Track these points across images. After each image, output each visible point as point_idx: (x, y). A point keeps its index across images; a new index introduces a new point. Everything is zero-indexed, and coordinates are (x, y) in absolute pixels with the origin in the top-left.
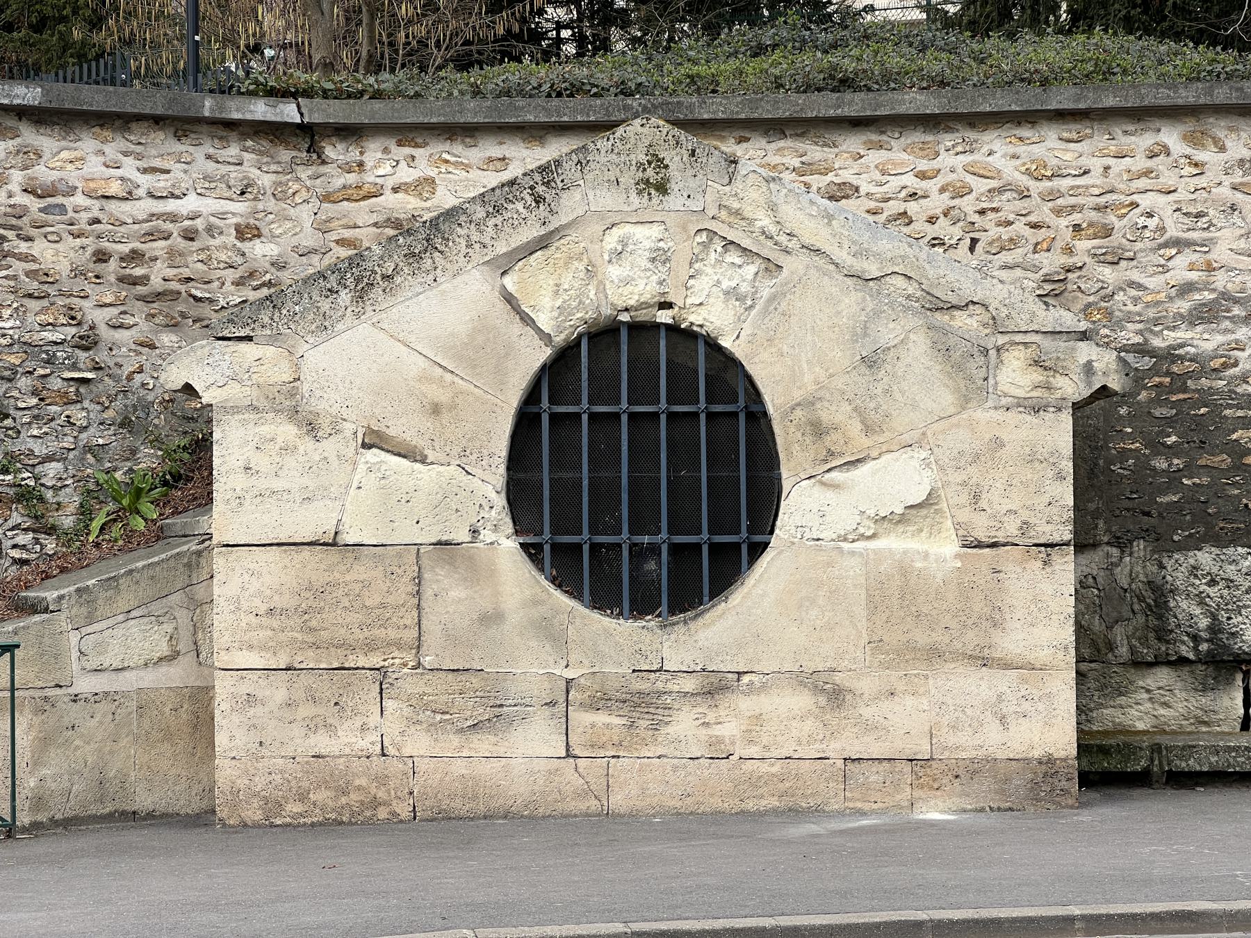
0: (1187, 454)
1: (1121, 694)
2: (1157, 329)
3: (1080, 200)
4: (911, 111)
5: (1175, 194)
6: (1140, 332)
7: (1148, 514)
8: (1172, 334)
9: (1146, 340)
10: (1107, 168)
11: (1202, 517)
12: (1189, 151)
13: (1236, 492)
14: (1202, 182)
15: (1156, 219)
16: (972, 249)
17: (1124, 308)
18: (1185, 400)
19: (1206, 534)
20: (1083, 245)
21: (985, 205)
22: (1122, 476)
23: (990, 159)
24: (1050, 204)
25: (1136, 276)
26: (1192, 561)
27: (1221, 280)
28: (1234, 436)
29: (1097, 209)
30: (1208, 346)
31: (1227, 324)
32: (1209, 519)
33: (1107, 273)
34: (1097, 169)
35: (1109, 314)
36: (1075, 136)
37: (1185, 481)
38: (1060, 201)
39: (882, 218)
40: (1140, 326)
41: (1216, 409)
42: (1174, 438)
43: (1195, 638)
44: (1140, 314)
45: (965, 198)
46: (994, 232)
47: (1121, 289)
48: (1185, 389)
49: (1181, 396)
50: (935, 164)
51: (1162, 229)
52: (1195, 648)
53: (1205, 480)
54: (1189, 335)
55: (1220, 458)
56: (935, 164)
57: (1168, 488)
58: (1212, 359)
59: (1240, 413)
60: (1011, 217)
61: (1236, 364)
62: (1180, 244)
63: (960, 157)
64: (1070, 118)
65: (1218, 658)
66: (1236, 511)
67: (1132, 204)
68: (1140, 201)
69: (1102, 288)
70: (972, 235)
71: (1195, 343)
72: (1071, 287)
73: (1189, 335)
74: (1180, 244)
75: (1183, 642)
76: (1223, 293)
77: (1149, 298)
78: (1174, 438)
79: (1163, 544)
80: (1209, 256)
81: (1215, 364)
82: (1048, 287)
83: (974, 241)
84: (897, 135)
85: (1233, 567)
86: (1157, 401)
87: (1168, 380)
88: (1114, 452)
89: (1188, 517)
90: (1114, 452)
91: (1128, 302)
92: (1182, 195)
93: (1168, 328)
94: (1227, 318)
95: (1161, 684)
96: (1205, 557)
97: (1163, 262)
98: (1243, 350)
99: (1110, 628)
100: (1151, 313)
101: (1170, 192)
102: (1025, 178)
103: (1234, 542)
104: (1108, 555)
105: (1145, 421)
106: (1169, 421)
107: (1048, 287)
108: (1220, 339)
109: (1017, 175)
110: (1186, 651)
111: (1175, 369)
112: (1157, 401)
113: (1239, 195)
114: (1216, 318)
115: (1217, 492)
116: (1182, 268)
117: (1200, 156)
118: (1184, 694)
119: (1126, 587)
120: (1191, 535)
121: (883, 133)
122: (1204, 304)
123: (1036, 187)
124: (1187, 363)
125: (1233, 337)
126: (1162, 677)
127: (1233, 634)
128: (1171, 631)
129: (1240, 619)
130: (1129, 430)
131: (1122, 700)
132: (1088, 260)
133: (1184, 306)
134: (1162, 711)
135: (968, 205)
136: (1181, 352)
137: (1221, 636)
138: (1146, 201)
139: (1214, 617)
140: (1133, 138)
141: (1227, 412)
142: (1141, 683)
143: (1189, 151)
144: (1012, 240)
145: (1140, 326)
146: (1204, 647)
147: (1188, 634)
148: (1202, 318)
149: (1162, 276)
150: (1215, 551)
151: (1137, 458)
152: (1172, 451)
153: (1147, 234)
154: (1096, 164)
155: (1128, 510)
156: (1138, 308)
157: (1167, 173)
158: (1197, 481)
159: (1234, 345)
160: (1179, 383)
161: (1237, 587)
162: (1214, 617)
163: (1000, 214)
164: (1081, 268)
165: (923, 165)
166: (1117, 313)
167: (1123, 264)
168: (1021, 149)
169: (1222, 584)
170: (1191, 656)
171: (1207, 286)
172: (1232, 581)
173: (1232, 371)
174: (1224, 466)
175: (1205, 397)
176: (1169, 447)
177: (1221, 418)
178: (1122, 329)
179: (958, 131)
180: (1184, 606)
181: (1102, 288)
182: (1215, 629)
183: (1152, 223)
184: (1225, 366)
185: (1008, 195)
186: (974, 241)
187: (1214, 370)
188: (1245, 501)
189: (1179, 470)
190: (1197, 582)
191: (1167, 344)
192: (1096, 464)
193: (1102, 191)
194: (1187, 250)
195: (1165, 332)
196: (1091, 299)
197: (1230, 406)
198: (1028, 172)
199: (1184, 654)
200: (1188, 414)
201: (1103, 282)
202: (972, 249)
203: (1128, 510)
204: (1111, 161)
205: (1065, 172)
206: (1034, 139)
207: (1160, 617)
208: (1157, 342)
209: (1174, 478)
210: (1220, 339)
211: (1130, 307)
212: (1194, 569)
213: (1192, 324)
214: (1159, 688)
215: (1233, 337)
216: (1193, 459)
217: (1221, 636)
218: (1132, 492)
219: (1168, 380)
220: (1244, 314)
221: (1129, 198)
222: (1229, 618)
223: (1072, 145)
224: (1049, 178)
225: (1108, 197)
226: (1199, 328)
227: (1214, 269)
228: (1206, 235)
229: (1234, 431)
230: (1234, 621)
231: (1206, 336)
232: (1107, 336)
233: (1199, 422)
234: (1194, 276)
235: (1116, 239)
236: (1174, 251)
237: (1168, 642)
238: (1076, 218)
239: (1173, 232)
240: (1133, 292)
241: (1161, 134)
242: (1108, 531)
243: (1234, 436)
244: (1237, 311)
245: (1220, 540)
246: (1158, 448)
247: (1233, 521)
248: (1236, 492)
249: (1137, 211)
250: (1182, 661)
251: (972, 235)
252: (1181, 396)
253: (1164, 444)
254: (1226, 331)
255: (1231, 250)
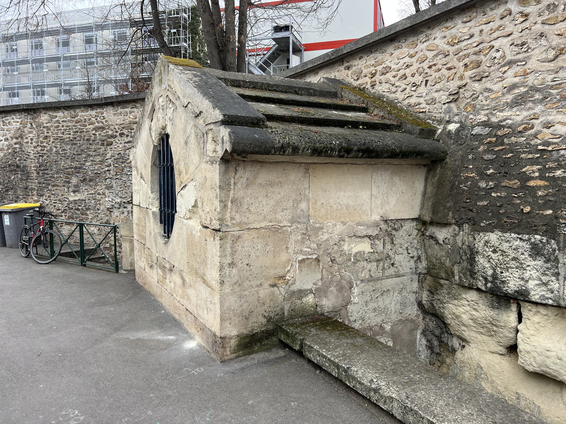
0: (497, 180)
1: (455, 299)
2: (495, 112)
3: (469, 51)
4: (401, 29)
5: (512, 36)
6: (487, 115)
7: (471, 211)
8: (501, 114)
9: (489, 119)
10: (481, 31)
11: (496, 215)
12: (521, 9)
13: (518, 202)
14: (526, 25)
15: (500, 53)
16: (426, 85)
17: (481, 103)
18: (502, 150)
19: (497, 224)
20: (469, 73)
21: (431, 64)
22: (464, 190)
23: (435, 41)
24: (456, 56)
25: (489, 85)
26: (486, 238)
27: (531, 80)
28: (524, 170)
29: (475, 54)
30: (519, 119)
31: (530, 104)
32: (500, 216)
33: (477, 86)
34: (477, 33)
35: (474, 107)
36: (468, 19)
37: (493, 194)
38: (461, 54)
39: (398, 78)
40: (487, 112)
41: (517, 154)
42: (491, 171)
43: (486, 279)
44: (488, 105)
45: (425, 62)
46: (434, 74)
47: (482, 93)
48: (502, 144)
49: (501, 148)
50: (416, 50)
51: (503, 57)
52: (486, 284)
53: (504, 194)
54: (510, 113)
55: (513, 182)
56: (416, 50)
57: (484, 198)
58: (520, 125)
59: (530, 156)
60: (440, 67)
61: (532, 128)
62: (511, 63)
63: (425, 44)
64: (467, 10)
65: (495, 293)
66: (516, 212)
67: (490, 47)
68: (494, 44)
69: (474, 94)
70: (426, 79)
71: (512, 117)
72: (461, 96)
73: (510, 113)
74: (511, 63)
75: (480, 280)
76: (532, 87)
77: (493, 96)
78: (491, 171)
79: (476, 228)
80: (526, 67)
81: (520, 129)
82: (451, 97)
83: (427, 81)
84: (404, 41)
85: (507, 244)
86: (487, 151)
87: (495, 139)
88: (463, 178)
89: (490, 214)
90: (463, 178)
91: (483, 100)
92: (516, 35)
93: (500, 111)
94: (530, 101)
95: (473, 299)
96: (493, 237)
97: (501, 75)
98: (537, 119)
99: (453, 265)
100: (493, 104)
101: (509, 35)
102: (448, 46)
103: (510, 230)
104: (454, 230)
105: (479, 162)
106: (491, 161)
107: (451, 97)
108: (525, 113)
109: (445, 46)
110: (480, 285)
111: (499, 133)
112: (487, 151)
113: (547, 27)
114: (524, 102)
115: (509, 200)
116: (511, 78)
117: (528, 10)
118: (484, 307)
119: (460, 246)
120: (490, 224)
121: (400, 41)
122: (520, 95)
123: (452, 49)
124: (506, 129)
125: (533, 111)
126: (472, 296)
127: (503, 281)
128: (476, 273)
129: (508, 274)
130: (471, 167)
131: (456, 302)
132: (468, 81)
133: (509, 98)
134: (474, 313)
135: (425, 65)
136: (504, 123)
137: (496, 281)
138: (496, 44)
139: (494, 270)
140: (495, 11)
141: (523, 156)
142: (464, 296)
143: (521, 9)
144: (439, 77)
145: (487, 112)
146: (489, 285)
147: (483, 277)
148: (517, 103)
149: (501, 83)
150: (500, 234)
151: (472, 181)
152: (490, 177)
153: (496, 61)
154: (476, 31)
155: (464, 207)
156: (487, 102)
157: (509, 25)
158: (499, 194)
159: (532, 117)
160: (500, 140)
161: (507, 256)
162: (494, 270)
163: (437, 66)
164: (465, 86)
165: (412, 52)
166: (478, 106)
167: (484, 80)
168: (447, 33)
169: (499, 253)
170: (483, 288)
171: (523, 84)
172: (505, 252)
173: (530, 132)
174: (515, 187)
175: (512, 148)
176: (489, 176)
177: (519, 159)
178: (479, 114)
179: (424, 32)
180: (481, 261)
181: (474, 94)
182: (495, 276)
183: (498, 55)
184: (526, 129)
185: (440, 56)
186: (427, 81)
187: (520, 132)
188: (522, 207)
189: (491, 188)
190: (488, 250)
191: (499, 119)
192: (455, 184)
193: (478, 43)
194: (514, 66)
195: (498, 113)
196: (469, 100)
197: (524, 152)
198: (448, 43)
199: (480, 287)
200: (502, 157)
201: (474, 91)
202: (426, 85)
203: (464, 207)
204: (484, 27)
205: (463, 39)
206: (452, 26)
207: (471, 265)
208: (494, 120)
209: (488, 191)
210: (525, 113)
211: (484, 102)
212: (487, 242)
213: (512, 107)
214: (472, 301)
215: (533, 111)
216: (500, 182)
217: (496, 281)
218: (467, 199)
219: (495, 139)
220: (541, 97)
221: (489, 44)
222: (502, 273)
223: (468, 23)
224: (457, 44)
225: (481, 46)
226: (515, 109)
227: (528, 74)
228: (526, 55)
229: (526, 166)
230: (504, 274)
231: (518, 113)
232: (471, 119)
233: (506, 162)
234: (517, 80)
235: (483, 67)
236: (507, 68)
237: (474, 278)
238: (466, 60)
239: (509, 57)
240: (486, 94)
241: (508, 4)
242: (453, 218)
243: (524, 170)
244: (538, 96)
245: (504, 229)
246: (483, 176)
247: (513, 218)
248: (518, 202)
249: (493, 50)
250: (479, 290)
251: (426, 79)
252: (501, 148)
253: (486, 174)
254: (530, 109)
255: (538, 60)
